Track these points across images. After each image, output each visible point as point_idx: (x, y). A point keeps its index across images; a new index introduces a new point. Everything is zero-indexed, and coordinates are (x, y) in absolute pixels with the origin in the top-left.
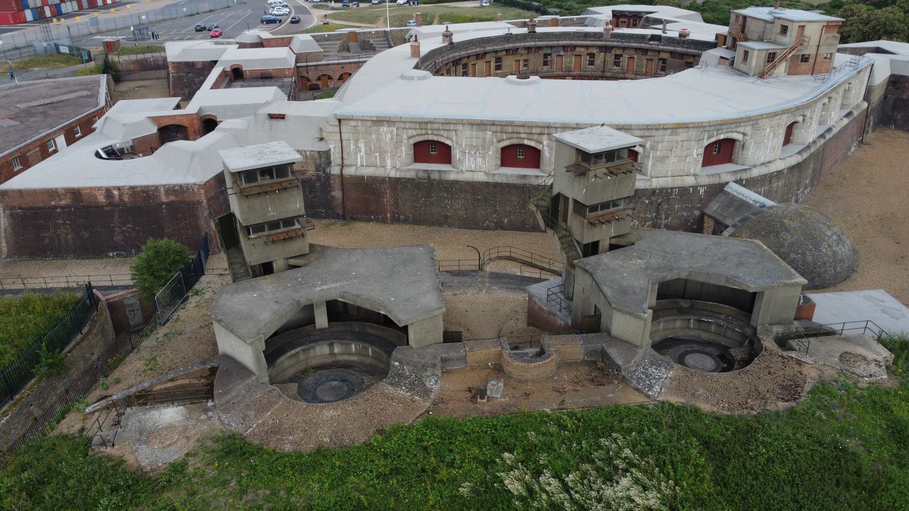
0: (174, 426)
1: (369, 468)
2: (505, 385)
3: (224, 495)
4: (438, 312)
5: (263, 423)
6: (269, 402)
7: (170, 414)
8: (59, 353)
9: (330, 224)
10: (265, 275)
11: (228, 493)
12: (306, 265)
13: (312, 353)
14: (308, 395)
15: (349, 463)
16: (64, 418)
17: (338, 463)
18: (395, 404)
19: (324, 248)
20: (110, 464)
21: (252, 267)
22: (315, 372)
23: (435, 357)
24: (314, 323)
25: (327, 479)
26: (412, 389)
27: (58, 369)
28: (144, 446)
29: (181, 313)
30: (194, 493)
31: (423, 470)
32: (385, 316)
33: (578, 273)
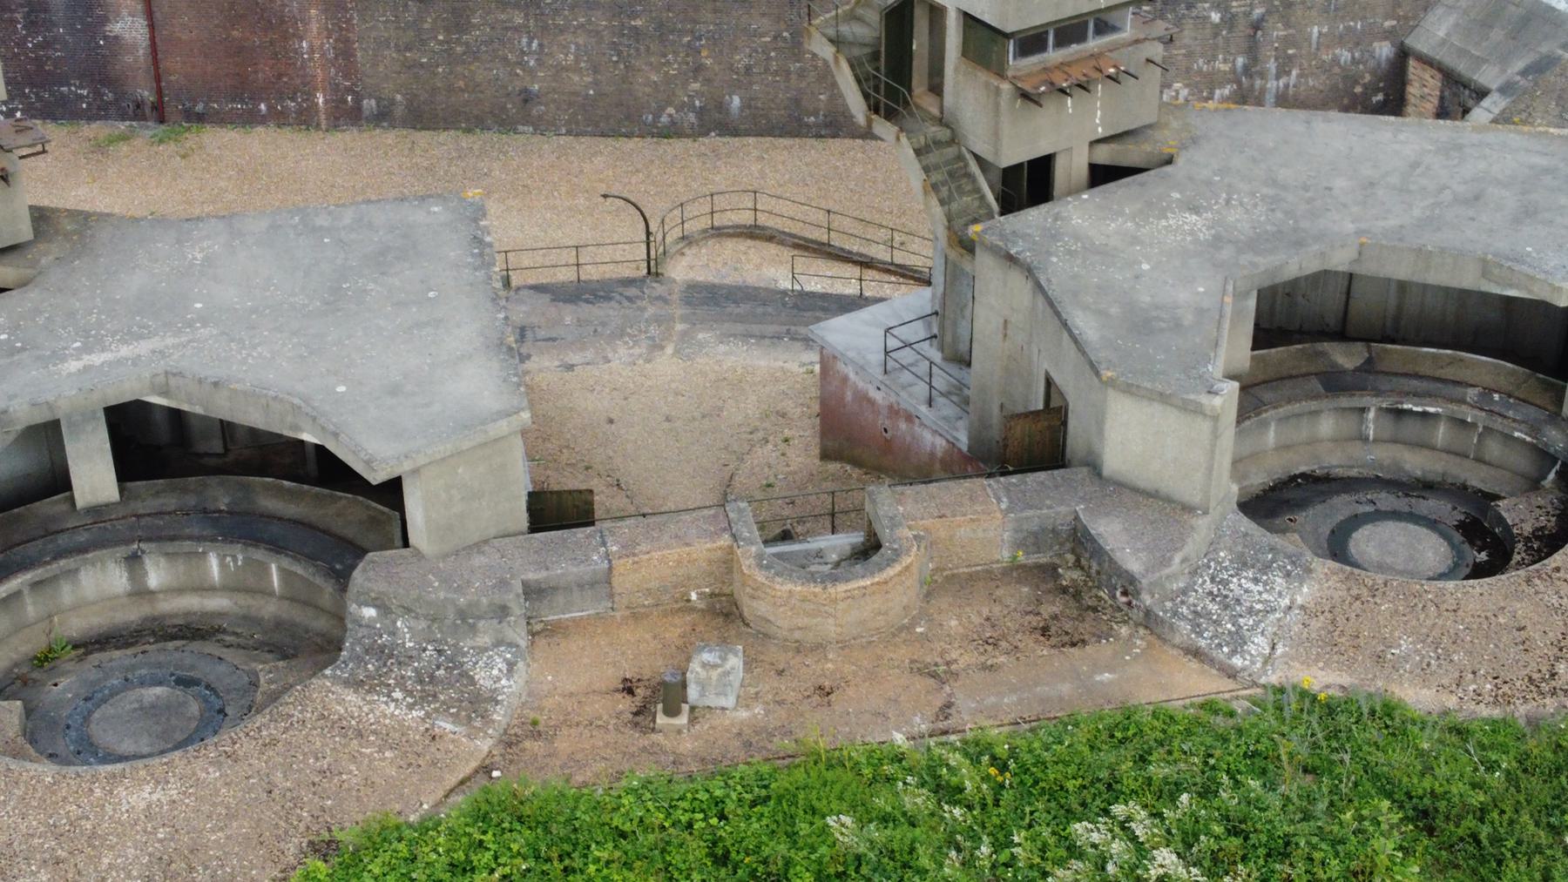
2: (749, 665)
4: (503, 427)
12: (23, 284)
13: (66, 594)
22: (80, 659)
23: (503, 584)
32: (321, 450)
33: (985, 266)
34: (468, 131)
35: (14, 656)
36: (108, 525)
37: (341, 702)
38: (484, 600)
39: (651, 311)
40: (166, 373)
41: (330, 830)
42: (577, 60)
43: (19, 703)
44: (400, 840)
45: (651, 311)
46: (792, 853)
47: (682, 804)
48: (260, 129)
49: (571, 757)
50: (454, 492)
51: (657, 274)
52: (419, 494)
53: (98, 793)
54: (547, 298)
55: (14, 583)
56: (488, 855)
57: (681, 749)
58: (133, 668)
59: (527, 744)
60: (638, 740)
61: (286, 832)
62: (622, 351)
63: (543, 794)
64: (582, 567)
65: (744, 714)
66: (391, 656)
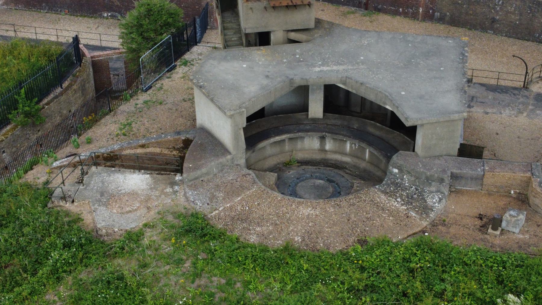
0: (137, 194)
1: (341, 278)
2: (527, 220)
3: (176, 275)
4: (456, 116)
5: (231, 208)
6: (241, 186)
7: (135, 181)
8: (38, 103)
9: (348, 13)
10: (260, 45)
11: (180, 273)
12: (308, 41)
13: (299, 145)
14: (284, 186)
15: (319, 269)
16: (32, 169)
17: (306, 266)
18: (385, 215)
19: (332, 24)
20: (66, 219)
21: (247, 35)
22: (298, 166)
23: (444, 171)
24: (307, 111)
25: (291, 280)
26: (408, 203)
27: (33, 119)
28: (103, 208)
29: (166, 82)
30: (145, 266)
31: (405, 295)
32: (392, 112)
34: (470, 29)
35: (278, 161)
36: (317, 125)
37: (379, 197)
38: (436, 175)
39: (521, 100)
40: (346, 77)
41: (365, 237)
42: (515, 10)
43: (276, 174)
44: (388, 246)
45: (521, 100)
46: (527, 287)
47: (492, 260)
48: (398, 17)
49: (454, 235)
50: (434, 136)
51: (527, 88)
52: (421, 134)
53: (294, 206)
54: (484, 88)
55: (284, 137)
56: (417, 259)
57: (495, 242)
58: (315, 172)
59: (440, 227)
60: (480, 236)
61: (351, 234)
62: (507, 111)
63: (441, 243)
64: (473, 172)
65: (521, 236)
66: (400, 187)
